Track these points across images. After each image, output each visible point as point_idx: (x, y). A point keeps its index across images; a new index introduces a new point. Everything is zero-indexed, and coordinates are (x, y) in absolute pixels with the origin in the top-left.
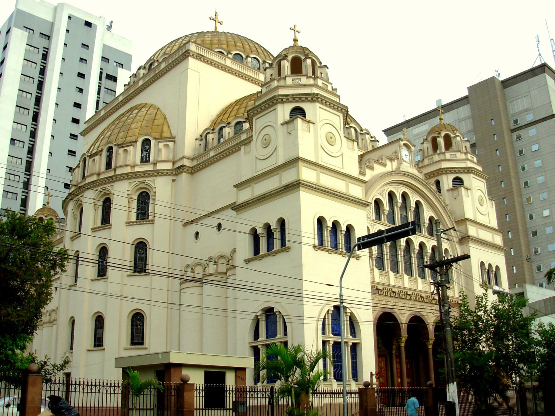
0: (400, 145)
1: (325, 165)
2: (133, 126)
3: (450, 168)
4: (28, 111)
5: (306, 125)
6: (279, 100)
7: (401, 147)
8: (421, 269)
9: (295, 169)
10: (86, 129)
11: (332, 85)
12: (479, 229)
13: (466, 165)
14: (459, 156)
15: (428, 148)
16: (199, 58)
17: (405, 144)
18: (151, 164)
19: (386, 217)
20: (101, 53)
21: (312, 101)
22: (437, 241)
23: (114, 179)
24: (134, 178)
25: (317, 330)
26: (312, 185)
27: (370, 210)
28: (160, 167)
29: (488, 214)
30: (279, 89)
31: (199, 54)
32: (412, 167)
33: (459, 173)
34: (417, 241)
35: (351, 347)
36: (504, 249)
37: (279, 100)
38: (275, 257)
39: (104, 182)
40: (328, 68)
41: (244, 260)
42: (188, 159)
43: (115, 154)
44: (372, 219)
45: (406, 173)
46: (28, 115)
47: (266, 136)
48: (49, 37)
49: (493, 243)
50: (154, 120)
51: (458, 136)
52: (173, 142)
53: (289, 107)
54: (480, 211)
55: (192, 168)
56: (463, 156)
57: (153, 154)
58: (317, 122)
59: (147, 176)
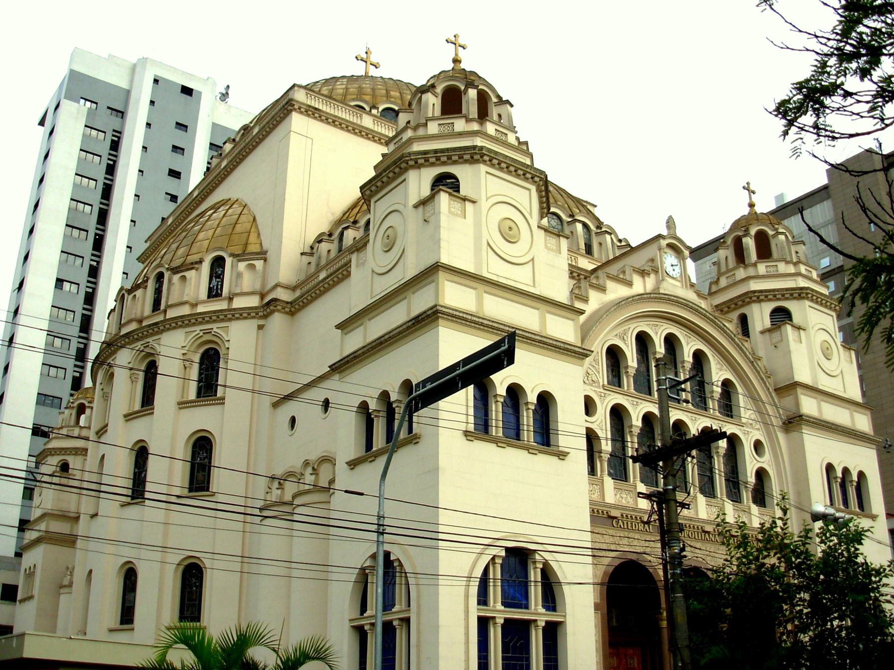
0: (660, 246)
1: (495, 278)
2: (201, 236)
3: (766, 291)
4: (86, 233)
5: (459, 205)
6: (412, 163)
7: (662, 251)
8: (706, 479)
9: (433, 284)
10: (146, 250)
11: (517, 135)
12: (855, 413)
13: (797, 285)
14: (782, 268)
15: (726, 257)
16: (311, 113)
17: (670, 246)
18: (224, 299)
19: (632, 380)
20: (209, 135)
21: (472, 161)
22: (659, 404)
23: (161, 328)
24: (194, 324)
25: (467, 596)
26: (465, 316)
27: (597, 366)
28: (238, 303)
29: (841, 375)
30: (412, 143)
31: (310, 106)
32: (686, 287)
33: (783, 300)
34: (637, 412)
35: (545, 629)
36: (874, 441)
37: (412, 163)
38: (374, 463)
39: (145, 333)
40: (512, 106)
41: (347, 463)
42: (286, 287)
43: (167, 286)
44: (601, 384)
45: (673, 298)
46: (86, 240)
47: (389, 230)
48: (121, 114)
49: (853, 428)
50: (236, 223)
51: (782, 233)
52: (263, 261)
53: (430, 174)
54: (827, 371)
55: (291, 303)
56: (791, 269)
57: (229, 281)
58: (480, 199)
59: (215, 321)
